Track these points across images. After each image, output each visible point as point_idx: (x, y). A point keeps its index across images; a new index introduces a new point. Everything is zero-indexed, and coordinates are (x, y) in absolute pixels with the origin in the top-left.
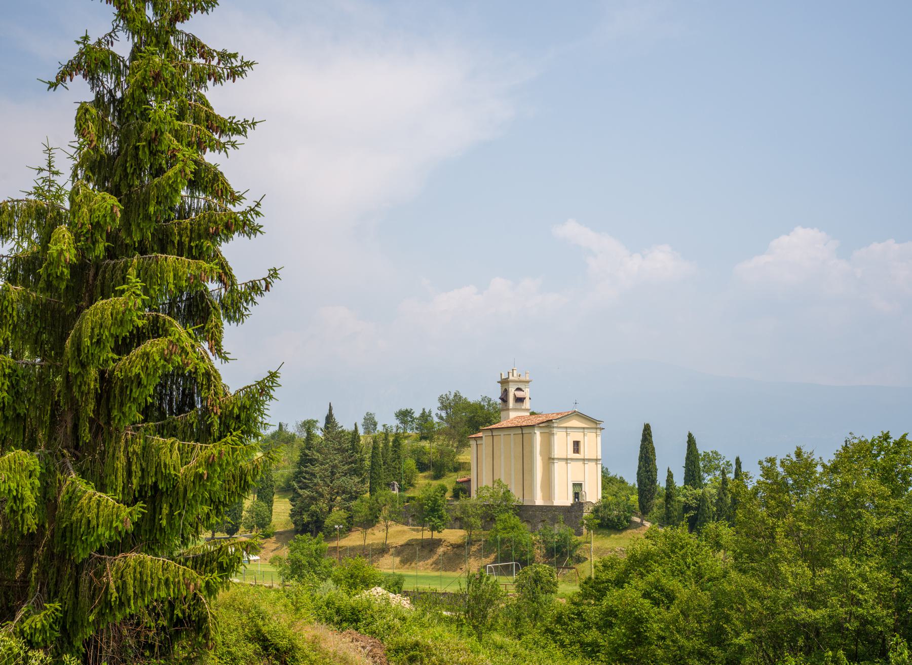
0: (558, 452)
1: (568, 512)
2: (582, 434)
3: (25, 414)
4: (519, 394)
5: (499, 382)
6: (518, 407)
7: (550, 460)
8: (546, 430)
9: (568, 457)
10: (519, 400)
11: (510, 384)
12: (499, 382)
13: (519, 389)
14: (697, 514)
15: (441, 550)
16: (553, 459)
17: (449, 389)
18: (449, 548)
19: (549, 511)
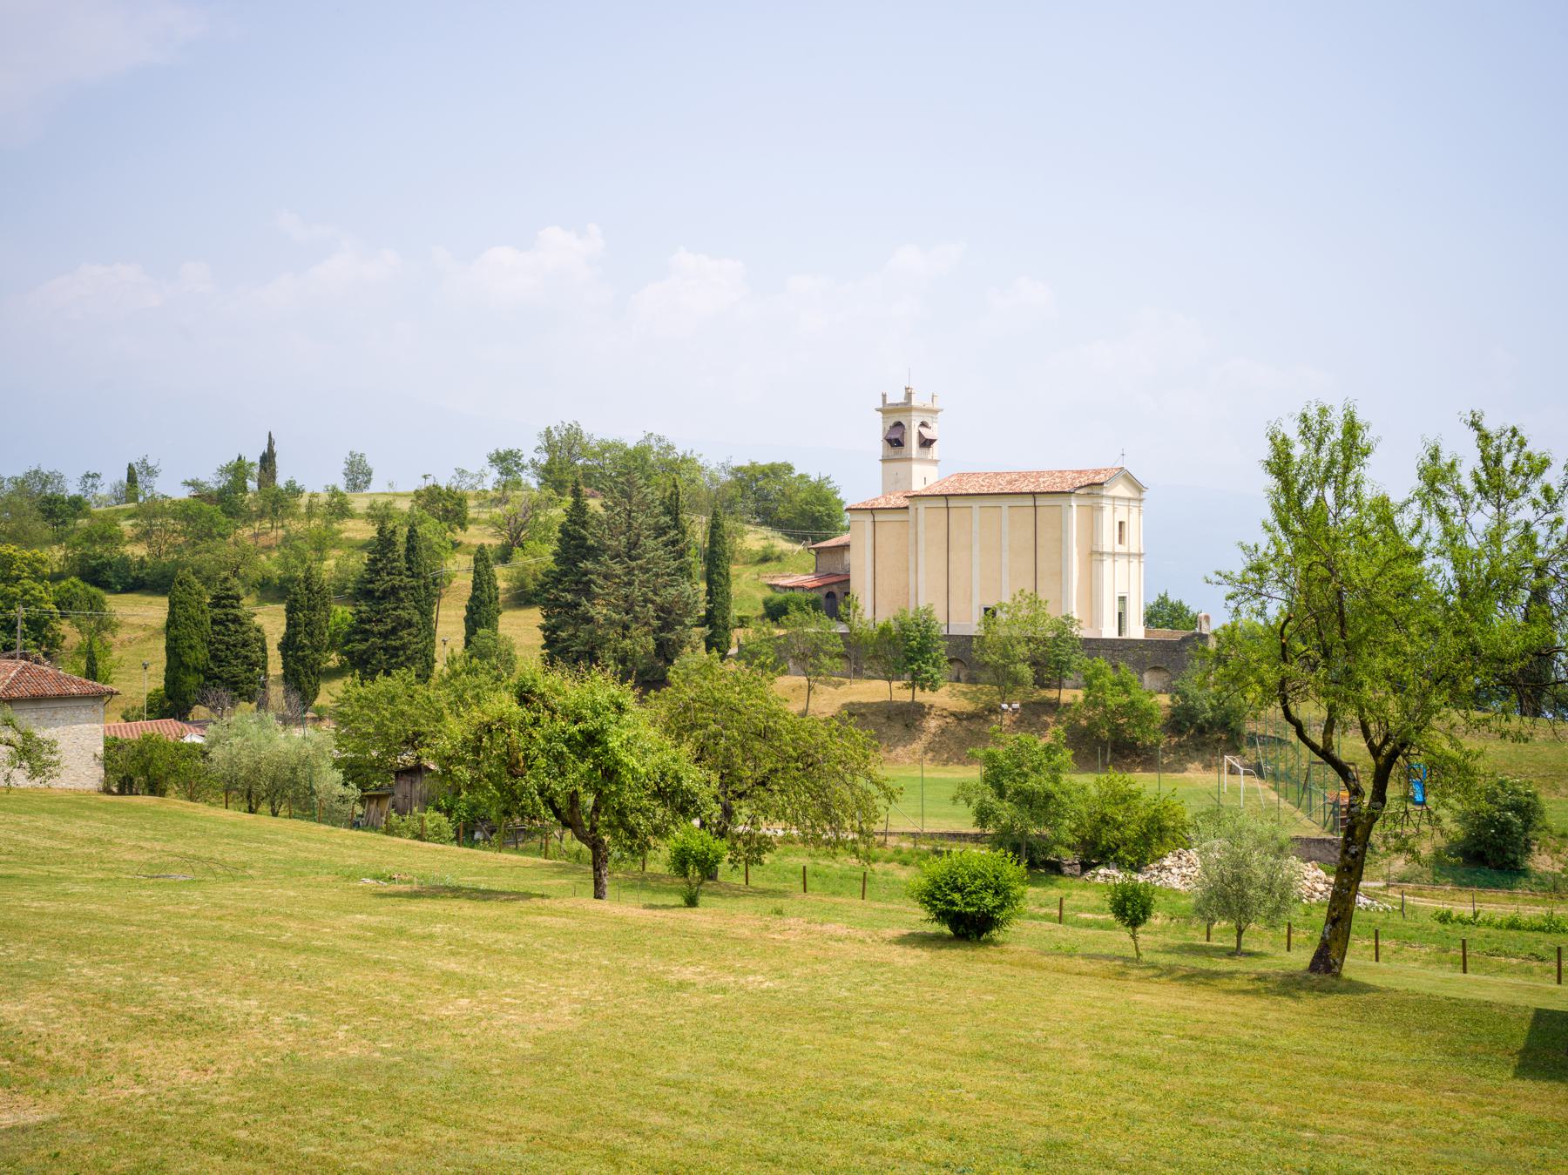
0: (1108, 541)
1: (1175, 650)
2: (1126, 509)
3: (597, 542)
4: (928, 434)
5: (878, 410)
6: (923, 456)
7: (1094, 555)
8: (1088, 502)
9: (1116, 551)
10: (926, 443)
11: (914, 413)
12: (878, 410)
13: (923, 424)
14: (713, 608)
15: (932, 724)
16: (1102, 554)
17: (558, 417)
18: (948, 720)
19: (1129, 649)
